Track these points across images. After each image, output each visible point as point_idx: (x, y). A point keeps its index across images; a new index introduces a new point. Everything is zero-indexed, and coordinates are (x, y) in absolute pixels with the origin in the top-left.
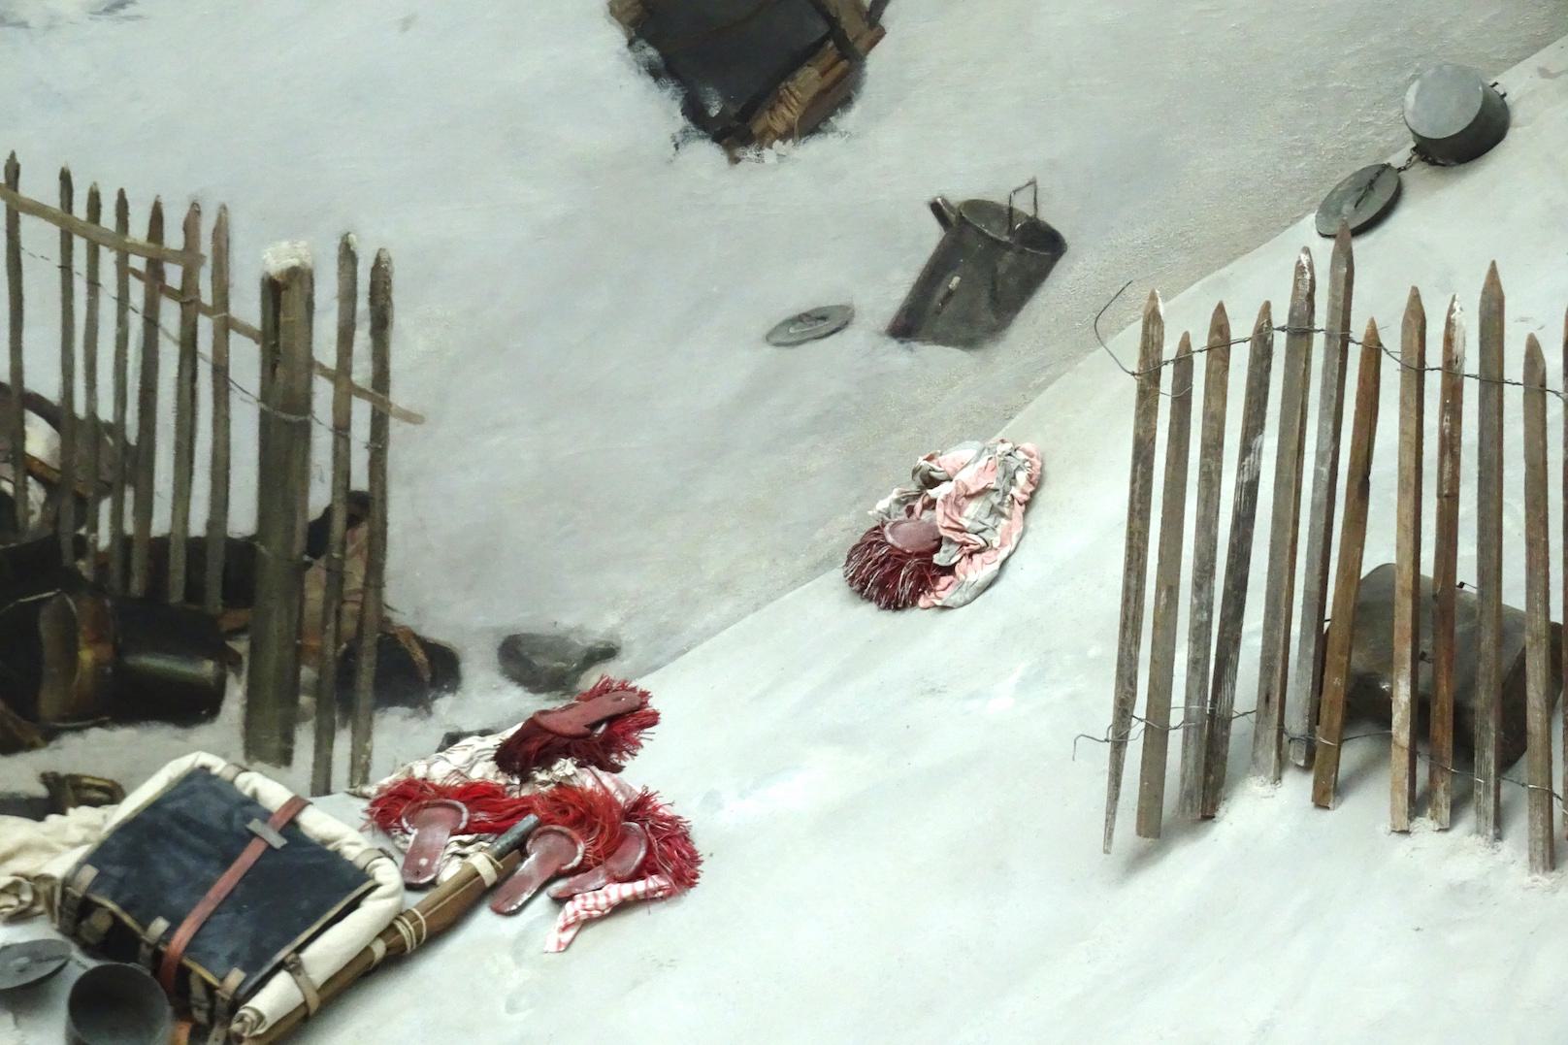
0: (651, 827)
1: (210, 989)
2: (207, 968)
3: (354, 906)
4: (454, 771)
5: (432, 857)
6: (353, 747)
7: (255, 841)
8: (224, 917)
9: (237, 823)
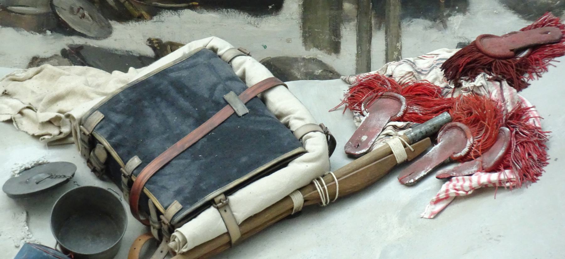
0: (517, 133)
1: (159, 213)
2: (158, 198)
3: (284, 164)
4: (410, 72)
5: (370, 137)
6: (387, 45)
7: (227, 108)
8: (182, 161)
9: (217, 94)
